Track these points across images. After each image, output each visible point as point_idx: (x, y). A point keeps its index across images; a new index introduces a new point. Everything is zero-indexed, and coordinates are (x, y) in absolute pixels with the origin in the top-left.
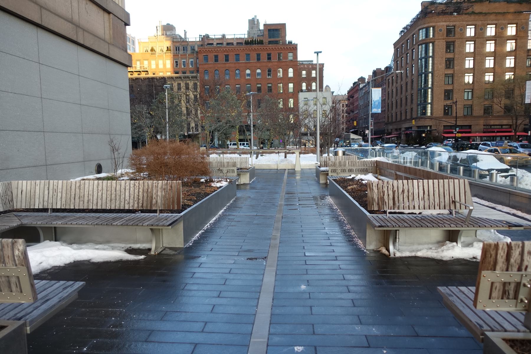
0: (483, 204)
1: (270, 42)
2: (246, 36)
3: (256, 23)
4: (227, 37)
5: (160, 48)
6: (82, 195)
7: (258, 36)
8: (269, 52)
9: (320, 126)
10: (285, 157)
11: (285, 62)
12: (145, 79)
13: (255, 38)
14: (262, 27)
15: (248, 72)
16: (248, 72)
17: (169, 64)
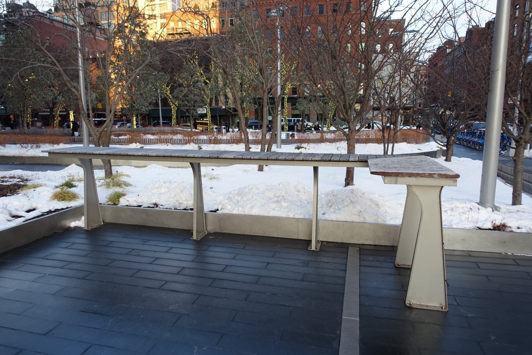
6: (142, 253)
10: (349, 180)
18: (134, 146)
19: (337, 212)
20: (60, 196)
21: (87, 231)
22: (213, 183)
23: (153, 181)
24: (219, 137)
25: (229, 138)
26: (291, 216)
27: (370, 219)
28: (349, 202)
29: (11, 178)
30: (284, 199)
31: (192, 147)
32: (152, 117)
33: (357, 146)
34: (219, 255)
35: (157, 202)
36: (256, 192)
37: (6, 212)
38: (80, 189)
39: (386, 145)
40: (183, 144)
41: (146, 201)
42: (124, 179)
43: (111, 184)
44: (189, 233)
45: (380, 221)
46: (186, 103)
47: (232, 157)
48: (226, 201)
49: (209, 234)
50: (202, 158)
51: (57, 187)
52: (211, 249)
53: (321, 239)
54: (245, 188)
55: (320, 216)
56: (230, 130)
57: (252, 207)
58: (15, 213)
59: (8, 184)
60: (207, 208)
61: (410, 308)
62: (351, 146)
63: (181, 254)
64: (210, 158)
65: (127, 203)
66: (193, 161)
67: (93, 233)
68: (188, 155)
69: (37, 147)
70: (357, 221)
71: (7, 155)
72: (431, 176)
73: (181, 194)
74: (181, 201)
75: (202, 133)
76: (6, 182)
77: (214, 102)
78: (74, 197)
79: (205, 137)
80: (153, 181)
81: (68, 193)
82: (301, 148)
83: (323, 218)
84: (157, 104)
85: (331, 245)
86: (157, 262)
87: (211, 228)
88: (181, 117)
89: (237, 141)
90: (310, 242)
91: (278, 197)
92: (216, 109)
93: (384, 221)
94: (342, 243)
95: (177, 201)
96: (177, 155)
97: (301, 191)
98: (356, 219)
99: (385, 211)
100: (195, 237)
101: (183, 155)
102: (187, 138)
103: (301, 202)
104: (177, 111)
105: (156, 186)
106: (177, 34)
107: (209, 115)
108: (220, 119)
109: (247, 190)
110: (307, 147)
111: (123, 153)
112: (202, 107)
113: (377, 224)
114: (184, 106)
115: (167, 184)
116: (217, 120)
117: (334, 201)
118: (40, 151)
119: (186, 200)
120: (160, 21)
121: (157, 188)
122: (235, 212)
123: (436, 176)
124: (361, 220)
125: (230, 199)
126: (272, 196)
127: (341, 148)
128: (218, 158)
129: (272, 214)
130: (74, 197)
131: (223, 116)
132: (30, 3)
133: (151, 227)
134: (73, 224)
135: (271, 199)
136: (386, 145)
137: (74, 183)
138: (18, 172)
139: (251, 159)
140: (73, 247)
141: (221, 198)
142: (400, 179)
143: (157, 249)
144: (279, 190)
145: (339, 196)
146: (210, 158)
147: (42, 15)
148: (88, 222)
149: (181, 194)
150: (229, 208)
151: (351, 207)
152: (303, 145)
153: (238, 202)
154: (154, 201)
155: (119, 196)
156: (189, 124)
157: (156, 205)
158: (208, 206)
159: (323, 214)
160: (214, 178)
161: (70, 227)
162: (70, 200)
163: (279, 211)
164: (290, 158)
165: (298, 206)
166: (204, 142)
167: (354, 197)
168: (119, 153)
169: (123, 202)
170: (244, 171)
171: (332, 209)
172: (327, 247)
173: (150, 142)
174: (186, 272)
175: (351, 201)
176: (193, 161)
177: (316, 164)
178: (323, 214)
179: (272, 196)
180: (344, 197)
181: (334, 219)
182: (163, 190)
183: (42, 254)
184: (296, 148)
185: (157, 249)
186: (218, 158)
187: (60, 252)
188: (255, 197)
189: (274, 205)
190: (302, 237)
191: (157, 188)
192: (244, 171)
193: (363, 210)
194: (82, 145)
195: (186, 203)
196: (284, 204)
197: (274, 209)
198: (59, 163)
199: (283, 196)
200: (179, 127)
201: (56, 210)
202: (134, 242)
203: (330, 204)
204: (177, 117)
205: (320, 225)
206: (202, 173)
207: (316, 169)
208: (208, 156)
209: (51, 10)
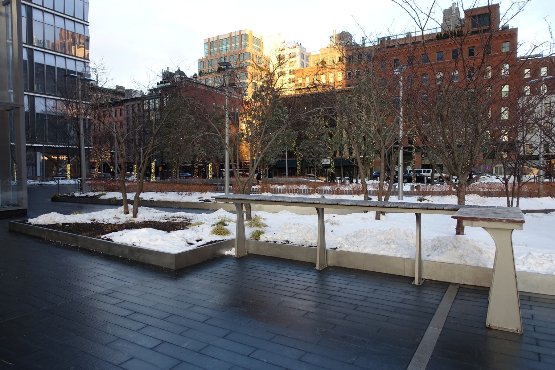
0: (134, 301)
1: (473, 33)
2: (440, 30)
3: (454, 12)
4: (413, 35)
5: (331, 60)
6: (278, 275)
7: (456, 27)
8: (472, 45)
9: (238, 192)
10: (460, 230)
12: (312, 95)
13: (452, 28)
14: (462, 16)
15: (440, 75)
16: (440, 75)
17: (340, 76)
18: (265, 194)
19: (440, 254)
20: (218, 232)
21: (236, 259)
22: (334, 228)
23: (285, 223)
24: (342, 188)
25: (350, 189)
26: (399, 256)
27: (471, 262)
28: (452, 246)
29: (178, 217)
30: (394, 242)
31: (316, 196)
32: (277, 168)
33: (467, 197)
34: (336, 281)
35: (289, 240)
36: (369, 235)
37: (184, 240)
38: (232, 227)
39: (510, 198)
40: (308, 194)
41: (280, 238)
42: (262, 221)
43: (253, 224)
44: (314, 265)
45: (481, 265)
46: (311, 155)
47: (349, 204)
48: (344, 241)
49: (329, 267)
50: (325, 204)
51: (214, 225)
52: (330, 276)
53: (425, 276)
54: (360, 231)
55: (424, 257)
56: (354, 181)
57: (365, 247)
58: (190, 241)
59: (177, 221)
60: (328, 247)
61: (489, 328)
62: (461, 198)
63: (307, 279)
64: (331, 204)
65: (266, 239)
66: (318, 206)
67: (241, 259)
68: (315, 202)
69: (190, 194)
70: (458, 263)
71: (169, 200)
72: (500, 221)
73: (307, 234)
74: (307, 240)
75: (325, 183)
76: (176, 220)
77: (338, 153)
78: (227, 233)
79: (328, 188)
80: (285, 223)
81: (223, 229)
82: (424, 200)
83: (427, 259)
84: (284, 156)
85: (433, 282)
86: (289, 281)
87: (330, 262)
88: (306, 168)
89: (358, 193)
90: (413, 278)
91: (388, 240)
92: (340, 159)
93: (484, 265)
94: (445, 282)
95: (304, 239)
96: (307, 201)
97: (409, 236)
98: (457, 261)
99: (488, 257)
100: (317, 268)
101: (311, 202)
102: (312, 189)
103: (408, 245)
104: (302, 162)
105: (288, 227)
106: (304, 89)
107: (333, 166)
108: (344, 169)
109: (362, 233)
110: (431, 199)
111: (267, 199)
112: (326, 158)
113: (477, 267)
114: (309, 157)
115: (296, 226)
116: (341, 171)
117: (439, 245)
118: (194, 198)
119: (311, 239)
120: (288, 77)
121: (288, 229)
122: (351, 250)
123: (504, 221)
124: (463, 262)
125: (347, 240)
126: (383, 239)
127: (452, 200)
128: (337, 204)
129: (382, 253)
130: (227, 233)
131: (347, 166)
132: (181, 70)
133: (283, 258)
134: (227, 253)
135: (382, 241)
136: (510, 198)
137: (226, 223)
138: (182, 214)
139: (363, 206)
140: (229, 267)
141: (340, 239)
142: (475, 223)
143: (289, 273)
144: (389, 234)
145: (444, 241)
146: (331, 204)
147: (189, 80)
148: (238, 252)
149: (307, 234)
150: (346, 247)
151: (454, 251)
152: (426, 197)
153: (354, 242)
154: (286, 239)
155: (260, 233)
156: (313, 175)
157: (288, 242)
158: (330, 243)
159: (428, 256)
160: (335, 223)
161: (224, 255)
162: (224, 235)
163: (387, 251)
164: (395, 206)
165: (405, 248)
166: (327, 192)
167: (457, 243)
168: (264, 199)
169: (262, 238)
170: (362, 219)
171: (436, 252)
172: (427, 284)
173: (279, 192)
174: (311, 289)
175: (454, 246)
176: (318, 206)
177: (418, 212)
178: (428, 256)
179: (383, 239)
180: (448, 242)
181: (437, 260)
182: (293, 231)
183: (210, 270)
184: (418, 200)
185: (289, 273)
186: (337, 204)
187: (220, 269)
188: (368, 239)
189: (384, 246)
190: (407, 274)
191: (288, 229)
192: (362, 219)
193: (466, 254)
194: (223, 194)
195: (311, 241)
196: (393, 246)
197: (384, 250)
198: (206, 208)
199: (393, 240)
200: (303, 178)
201: (216, 241)
202: (272, 268)
203: (435, 248)
204: (301, 168)
205: (424, 264)
206: (325, 219)
207: (418, 217)
208: (330, 203)
209: (196, 74)
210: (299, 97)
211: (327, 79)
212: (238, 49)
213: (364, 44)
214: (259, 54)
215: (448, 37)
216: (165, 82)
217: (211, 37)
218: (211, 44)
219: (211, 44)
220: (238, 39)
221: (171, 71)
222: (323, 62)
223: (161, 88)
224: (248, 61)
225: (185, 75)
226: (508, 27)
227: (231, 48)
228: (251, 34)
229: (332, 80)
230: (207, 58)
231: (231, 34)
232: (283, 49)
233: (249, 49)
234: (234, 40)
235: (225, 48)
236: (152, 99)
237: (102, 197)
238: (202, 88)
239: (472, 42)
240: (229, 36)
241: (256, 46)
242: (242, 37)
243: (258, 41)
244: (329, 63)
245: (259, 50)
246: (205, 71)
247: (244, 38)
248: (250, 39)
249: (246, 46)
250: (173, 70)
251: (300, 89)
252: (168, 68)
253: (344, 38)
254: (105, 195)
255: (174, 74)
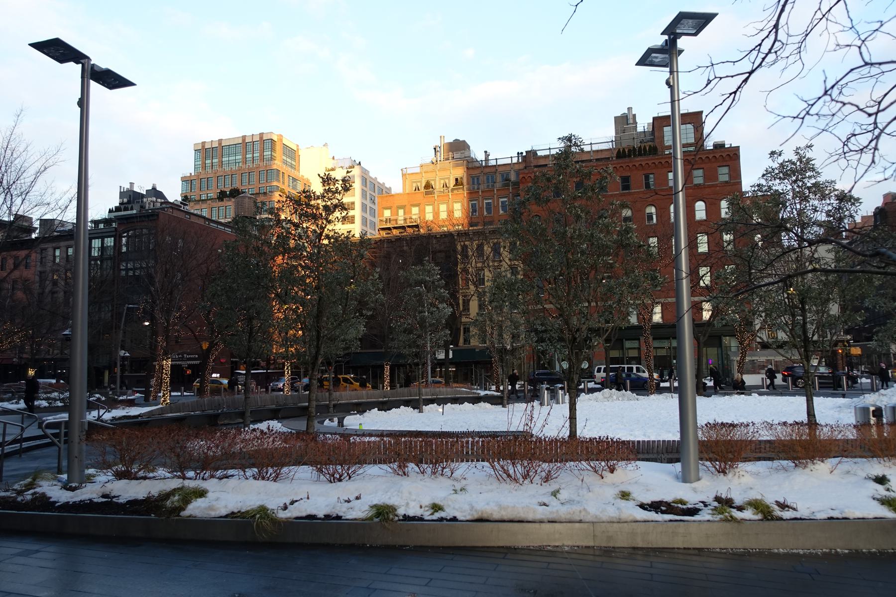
3: (631, 121)
11: (713, 186)
17: (458, 210)
106: (395, 228)
210: (389, 241)
211: (436, 213)
212: (256, 162)
213: (487, 160)
214: (293, 173)
215: (640, 155)
216: (126, 209)
217: (208, 140)
218: (205, 152)
219: (205, 152)
220: (257, 147)
221: (136, 189)
222: (428, 186)
223: (119, 219)
224: (275, 183)
225: (164, 198)
226: (724, 145)
227: (245, 161)
228: (281, 140)
229: (429, 217)
230: (198, 175)
231: (244, 137)
232: (333, 170)
233: (277, 164)
234: (250, 148)
235: (233, 160)
236: (98, 238)
237: (196, 508)
238: (201, 222)
239: (707, 160)
240: (241, 141)
241: (289, 160)
242: (266, 143)
243: (292, 154)
244: (438, 186)
245: (292, 166)
246: (194, 196)
247: (268, 145)
248: (278, 148)
249: (272, 158)
250: (142, 187)
251: (389, 229)
252: (132, 184)
253: (458, 148)
254: (202, 493)
255: (142, 196)
